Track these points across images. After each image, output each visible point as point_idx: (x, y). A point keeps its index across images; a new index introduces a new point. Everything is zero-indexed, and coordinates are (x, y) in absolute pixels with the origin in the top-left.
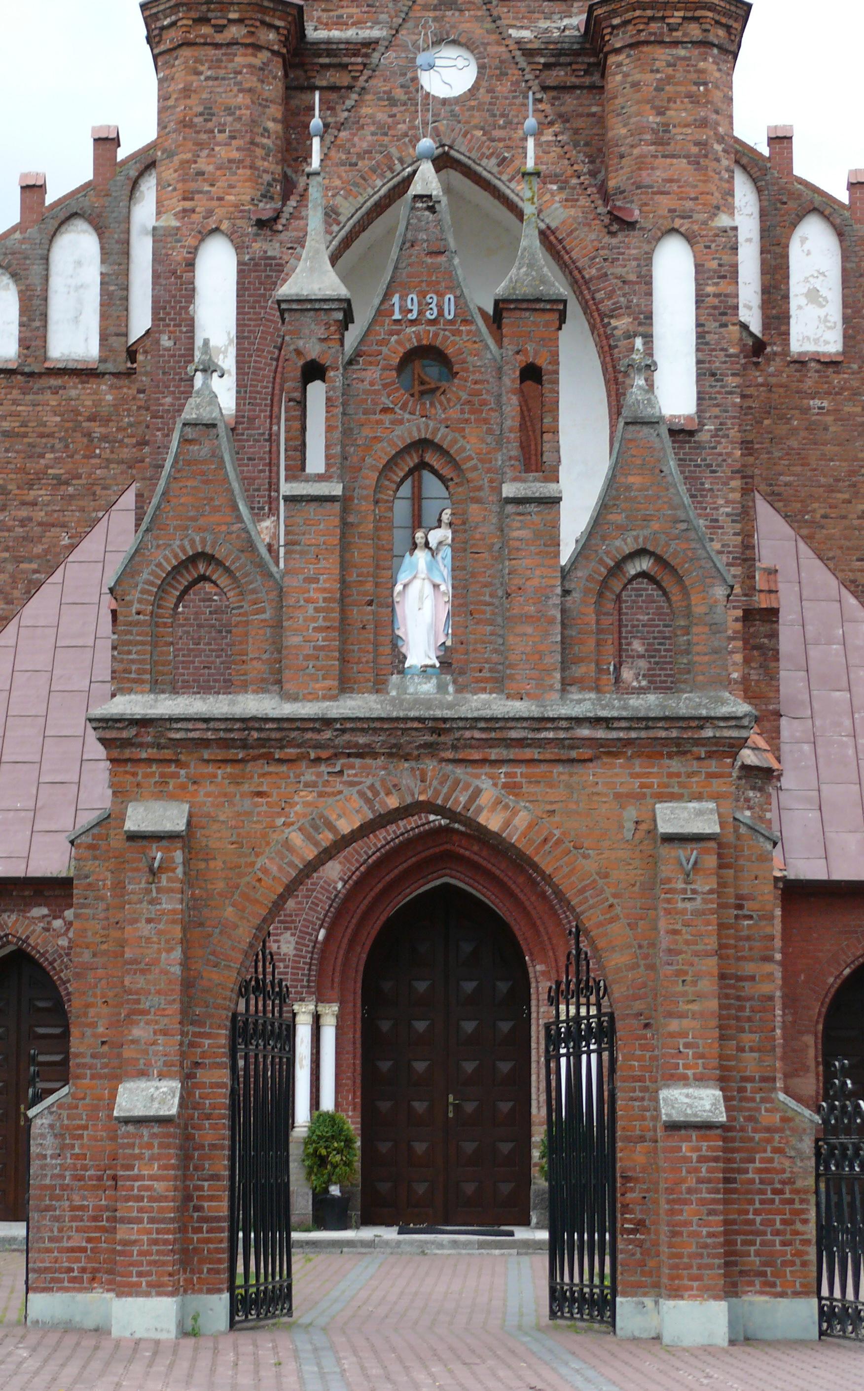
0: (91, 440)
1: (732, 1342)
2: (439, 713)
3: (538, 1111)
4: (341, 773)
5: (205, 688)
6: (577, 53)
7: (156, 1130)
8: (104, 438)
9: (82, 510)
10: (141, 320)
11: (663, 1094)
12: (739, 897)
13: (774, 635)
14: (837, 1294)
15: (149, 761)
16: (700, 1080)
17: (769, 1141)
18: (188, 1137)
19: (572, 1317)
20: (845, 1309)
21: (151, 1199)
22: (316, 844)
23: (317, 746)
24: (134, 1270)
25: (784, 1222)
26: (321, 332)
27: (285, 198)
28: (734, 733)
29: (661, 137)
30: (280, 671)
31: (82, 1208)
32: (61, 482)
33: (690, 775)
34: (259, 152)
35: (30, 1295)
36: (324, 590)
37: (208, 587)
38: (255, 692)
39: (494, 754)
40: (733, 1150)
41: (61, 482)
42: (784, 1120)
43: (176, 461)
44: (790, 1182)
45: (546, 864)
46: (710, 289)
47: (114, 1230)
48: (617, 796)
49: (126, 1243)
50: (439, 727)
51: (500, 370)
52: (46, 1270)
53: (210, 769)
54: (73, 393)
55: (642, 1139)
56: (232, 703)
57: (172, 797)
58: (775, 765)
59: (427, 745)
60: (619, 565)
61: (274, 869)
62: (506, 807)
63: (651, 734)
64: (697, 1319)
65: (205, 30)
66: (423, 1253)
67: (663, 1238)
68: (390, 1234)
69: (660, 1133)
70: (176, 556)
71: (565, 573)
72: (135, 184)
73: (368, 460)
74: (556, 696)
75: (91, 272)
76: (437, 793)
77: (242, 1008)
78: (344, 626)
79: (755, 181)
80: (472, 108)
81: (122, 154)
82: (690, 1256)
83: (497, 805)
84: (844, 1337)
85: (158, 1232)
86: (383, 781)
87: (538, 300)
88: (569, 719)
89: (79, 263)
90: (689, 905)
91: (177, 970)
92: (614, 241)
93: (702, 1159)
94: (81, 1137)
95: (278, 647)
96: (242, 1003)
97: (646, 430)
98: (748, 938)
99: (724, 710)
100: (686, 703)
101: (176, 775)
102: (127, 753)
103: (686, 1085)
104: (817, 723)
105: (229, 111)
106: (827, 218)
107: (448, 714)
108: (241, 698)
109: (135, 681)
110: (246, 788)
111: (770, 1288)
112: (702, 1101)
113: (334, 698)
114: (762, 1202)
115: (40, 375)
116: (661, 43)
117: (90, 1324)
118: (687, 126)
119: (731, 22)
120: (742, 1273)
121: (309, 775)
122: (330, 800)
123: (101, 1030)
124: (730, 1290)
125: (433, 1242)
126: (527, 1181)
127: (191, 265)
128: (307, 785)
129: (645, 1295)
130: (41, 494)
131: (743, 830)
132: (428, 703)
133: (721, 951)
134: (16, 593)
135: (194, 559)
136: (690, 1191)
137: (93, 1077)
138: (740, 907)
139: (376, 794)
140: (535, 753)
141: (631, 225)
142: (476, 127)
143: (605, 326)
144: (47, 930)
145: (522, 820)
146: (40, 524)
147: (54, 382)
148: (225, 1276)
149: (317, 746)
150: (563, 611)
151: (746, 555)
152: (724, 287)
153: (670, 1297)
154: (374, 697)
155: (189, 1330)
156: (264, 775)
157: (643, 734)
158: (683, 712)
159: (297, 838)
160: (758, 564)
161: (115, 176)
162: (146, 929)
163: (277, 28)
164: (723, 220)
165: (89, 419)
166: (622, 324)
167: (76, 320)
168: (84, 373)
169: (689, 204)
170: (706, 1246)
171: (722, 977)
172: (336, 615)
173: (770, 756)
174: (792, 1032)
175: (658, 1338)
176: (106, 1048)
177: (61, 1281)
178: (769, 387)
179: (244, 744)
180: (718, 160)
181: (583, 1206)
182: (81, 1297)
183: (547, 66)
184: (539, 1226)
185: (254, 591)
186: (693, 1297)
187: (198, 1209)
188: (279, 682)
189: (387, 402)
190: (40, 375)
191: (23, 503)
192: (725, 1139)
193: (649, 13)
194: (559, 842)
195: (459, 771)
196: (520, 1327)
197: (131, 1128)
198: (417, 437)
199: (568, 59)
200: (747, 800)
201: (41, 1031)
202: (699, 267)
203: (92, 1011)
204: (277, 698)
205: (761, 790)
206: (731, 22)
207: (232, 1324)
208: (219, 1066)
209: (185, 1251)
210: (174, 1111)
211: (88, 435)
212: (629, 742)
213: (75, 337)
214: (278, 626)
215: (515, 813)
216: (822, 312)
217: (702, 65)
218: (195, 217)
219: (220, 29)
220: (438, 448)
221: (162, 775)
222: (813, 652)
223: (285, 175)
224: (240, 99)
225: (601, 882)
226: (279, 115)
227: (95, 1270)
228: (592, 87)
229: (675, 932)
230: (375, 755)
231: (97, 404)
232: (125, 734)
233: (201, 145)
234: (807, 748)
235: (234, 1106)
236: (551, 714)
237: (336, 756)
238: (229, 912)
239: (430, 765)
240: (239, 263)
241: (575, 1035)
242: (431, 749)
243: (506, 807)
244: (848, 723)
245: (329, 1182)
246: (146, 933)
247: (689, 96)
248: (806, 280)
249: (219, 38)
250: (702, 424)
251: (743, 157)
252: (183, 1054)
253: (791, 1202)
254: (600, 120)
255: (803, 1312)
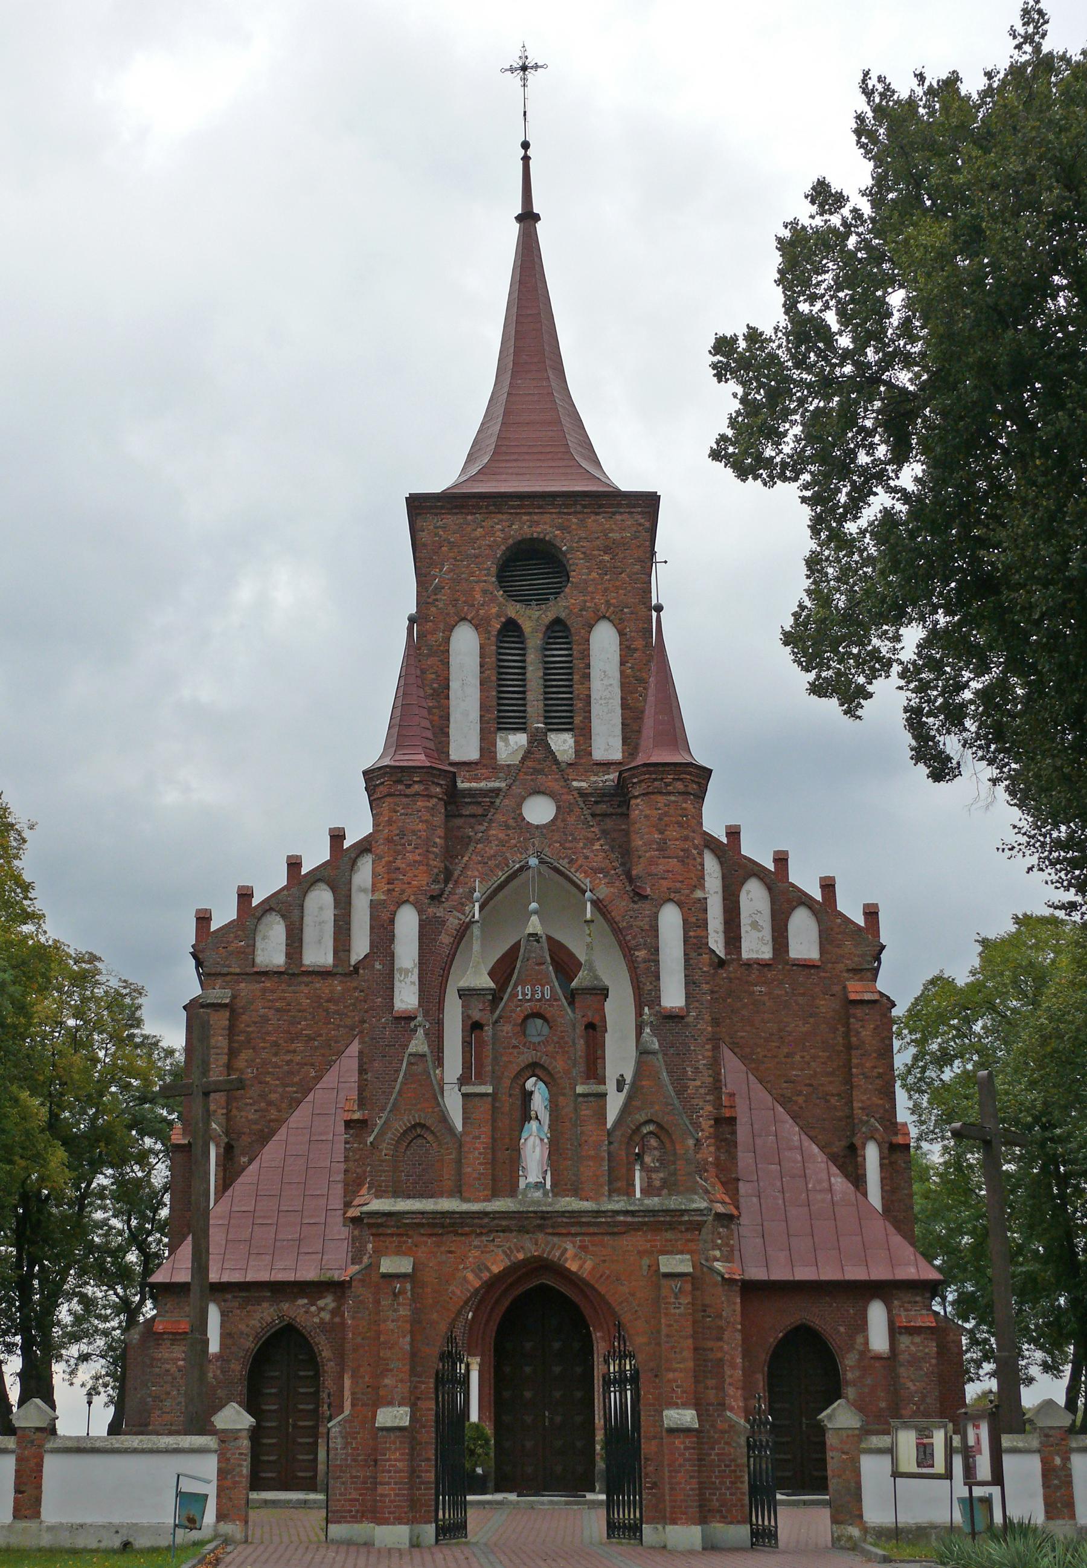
0: (328, 1013)
1: (704, 1549)
2: (544, 1209)
3: (599, 1422)
4: (493, 1240)
5: (421, 1195)
6: (613, 795)
7: (398, 1434)
8: (336, 1012)
9: (323, 1055)
10: (360, 946)
11: (665, 1413)
12: (704, 1305)
13: (734, 1133)
14: (760, 1522)
15: (392, 1235)
16: (685, 1405)
17: (723, 1438)
18: (414, 1438)
19: (619, 1537)
20: (764, 1530)
21: (395, 1472)
22: (480, 1278)
23: (482, 1226)
24: (386, 1510)
25: (731, 1482)
26: (481, 1007)
27: (446, 882)
28: (699, 1218)
29: (662, 847)
30: (460, 1186)
31: (356, 1477)
32: (311, 1039)
33: (676, 1241)
34: (432, 856)
35: (329, 1525)
36: (484, 1143)
37: (420, 1141)
38: (447, 1197)
39: (573, 1230)
40: (702, 1443)
41: (311, 1039)
42: (729, 1426)
43: (405, 1074)
44: (734, 1460)
45: (601, 1289)
46: (691, 934)
47: (376, 1489)
48: (639, 1252)
49: (382, 1495)
50: (544, 1216)
51: (574, 1025)
52: (337, 1511)
53: (425, 1239)
54: (318, 985)
55: (655, 1438)
56: (436, 1204)
57: (405, 1254)
58: (736, 1213)
59: (539, 1226)
60: (638, 1128)
61: (459, 1293)
62: (581, 1258)
63: (656, 1219)
64: (686, 1535)
65: (400, 787)
66: (532, 1508)
67: (667, 1491)
68: (512, 1497)
69: (664, 1434)
70: (405, 1125)
71: (610, 1133)
72: (354, 862)
73: (506, 1074)
74: (606, 1199)
75: (329, 914)
76: (544, 1251)
77: (441, 1366)
78: (494, 1162)
79: (718, 857)
80: (553, 831)
81: (347, 844)
82: (681, 1501)
83: (574, 1258)
84: (764, 1546)
85: (400, 1489)
86: (515, 1244)
87: (594, 989)
88: (613, 1211)
89: (321, 908)
90: (677, 1311)
91: (408, 1347)
92: (636, 906)
93: (686, 1448)
94: (356, 1438)
95: (459, 1173)
96: (441, 1365)
97: (651, 1056)
98: (709, 1328)
99: (694, 1206)
100: (674, 1202)
101: (406, 1242)
102: (381, 1230)
103: (678, 1408)
104: (761, 1184)
105: (414, 832)
106: (761, 879)
107: (549, 1209)
108: (440, 1200)
109: (384, 1191)
110: (443, 1249)
111: (724, 1519)
112: (685, 1417)
113: (489, 1201)
114: (719, 1472)
115: (298, 975)
116: (661, 793)
117: (361, 1540)
118: (677, 840)
119: (700, 780)
120: (709, 1511)
121: (476, 1243)
122: (488, 1255)
123: (367, 1379)
124: (703, 1520)
125: (538, 1502)
126: (593, 1463)
127: (392, 921)
128: (476, 1247)
129: (658, 1523)
130: (299, 1046)
131: (705, 1269)
132: (538, 1203)
133: (694, 1336)
134: (284, 1105)
135: (414, 1127)
136: (680, 1466)
137: (362, 1405)
138: (705, 1311)
139: (512, 1252)
140: (592, 1230)
141: (646, 897)
142: (557, 842)
143: (632, 955)
144: (306, 1312)
145: (589, 1265)
146: (298, 1064)
147: (306, 979)
148: (433, 1514)
149: (482, 1226)
150: (609, 1153)
151: (717, 1086)
152: (700, 932)
153: (670, 1524)
154: (509, 1200)
155: (415, 1544)
156: (452, 1242)
157: (652, 1219)
158: (672, 1207)
159: (470, 1276)
160: (724, 1089)
161: (343, 856)
162: (391, 1325)
163: (441, 785)
164: (699, 894)
165: (327, 1001)
166: (641, 954)
167: (320, 942)
168: (324, 974)
169: (678, 885)
170: (689, 1496)
171: (696, 1349)
172: (490, 1156)
173: (732, 1207)
174: (748, 1373)
175: (664, 1547)
176: (370, 1389)
177: (345, 1517)
178: (730, 980)
179: (442, 1226)
180: (695, 859)
181: (625, 1476)
182: (356, 1526)
183: (596, 802)
184: (600, 1492)
185: (447, 1143)
186: (682, 1524)
187: (419, 1477)
188: (460, 1192)
189: (514, 1042)
190: (298, 975)
191: (289, 1052)
192: (698, 1438)
193: (654, 776)
194: (608, 1277)
195: (556, 1239)
196: (591, 1543)
197: (384, 1433)
198: (531, 1061)
199: (607, 799)
200: (719, 1233)
201: (302, 1373)
202: (685, 921)
203: (362, 1370)
204: (459, 1201)
205: (727, 1227)
206: (700, 780)
207: (437, 1541)
208: (431, 1399)
209: (412, 1500)
210: (407, 1424)
211: (326, 1010)
212: (645, 1224)
213: (319, 953)
214: (459, 1162)
215: (584, 1262)
216: (760, 935)
217: (684, 805)
218: (394, 894)
219: (409, 786)
220: (542, 1067)
221: (399, 1242)
222: (758, 1141)
223: (446, 868)
224: (420, 826)
225: (631, 1299)
226: (442, 835)
227: (363, 1512)
228: (622, 814)
229: (670, 1326)
230: (511, 1231)
231: (331, 992)
232: (379, 1221)
233: (398, 853)
234: (755, 1200)
235: (437, 1422)
236: (603, 1209)
237: (491, 1231)
238: (435, 1316)
239: (540, 1236)
240: (420, 920)
241: (621, 1381)
242: (540, 1228)
243: (581, 1258)
244: (779, 1184)
245: (476, 1465)
246: (391, 1327)
247: (678, 823)
248: (750, 916)
249: (408, 791)
250: (688, 1012)
251: (710, 843)
252: (411, 1392)
253: (735, 1471)
254: (627, 833)
255: (741, 1532)
